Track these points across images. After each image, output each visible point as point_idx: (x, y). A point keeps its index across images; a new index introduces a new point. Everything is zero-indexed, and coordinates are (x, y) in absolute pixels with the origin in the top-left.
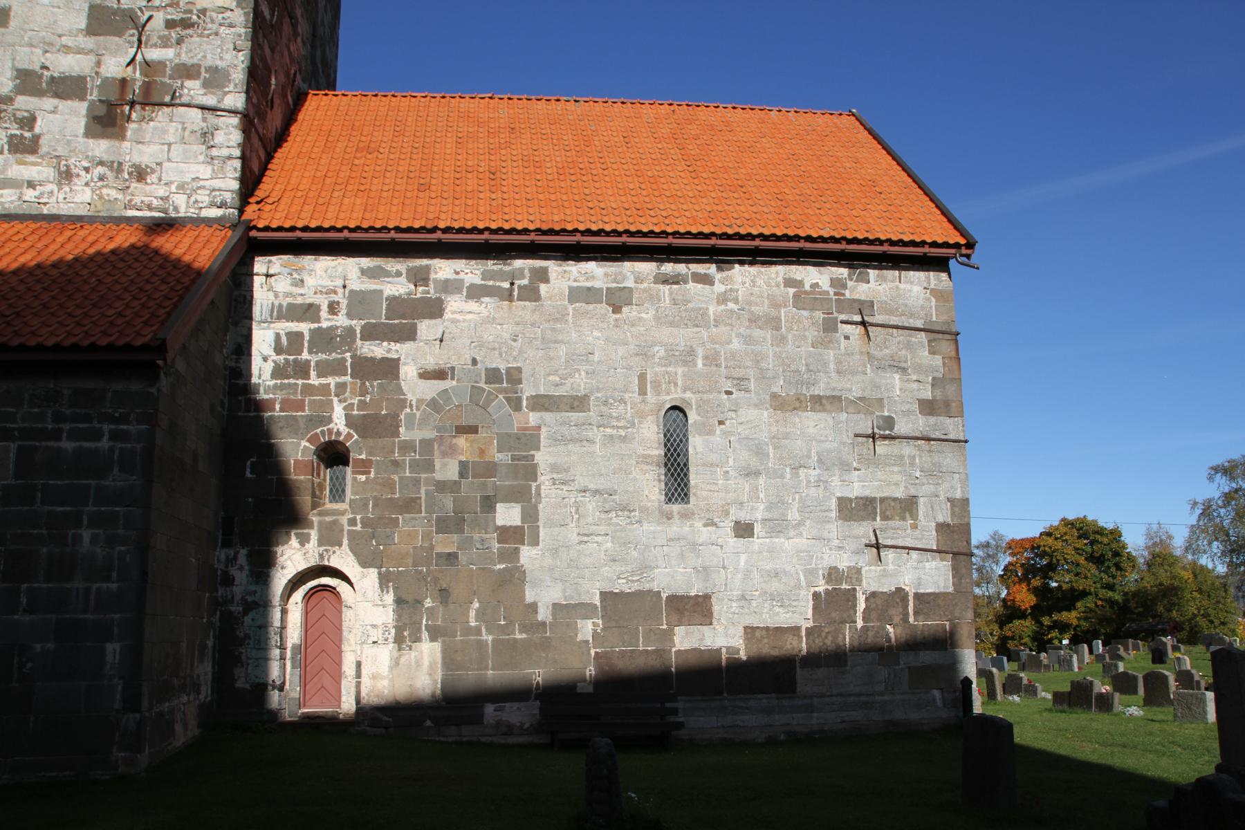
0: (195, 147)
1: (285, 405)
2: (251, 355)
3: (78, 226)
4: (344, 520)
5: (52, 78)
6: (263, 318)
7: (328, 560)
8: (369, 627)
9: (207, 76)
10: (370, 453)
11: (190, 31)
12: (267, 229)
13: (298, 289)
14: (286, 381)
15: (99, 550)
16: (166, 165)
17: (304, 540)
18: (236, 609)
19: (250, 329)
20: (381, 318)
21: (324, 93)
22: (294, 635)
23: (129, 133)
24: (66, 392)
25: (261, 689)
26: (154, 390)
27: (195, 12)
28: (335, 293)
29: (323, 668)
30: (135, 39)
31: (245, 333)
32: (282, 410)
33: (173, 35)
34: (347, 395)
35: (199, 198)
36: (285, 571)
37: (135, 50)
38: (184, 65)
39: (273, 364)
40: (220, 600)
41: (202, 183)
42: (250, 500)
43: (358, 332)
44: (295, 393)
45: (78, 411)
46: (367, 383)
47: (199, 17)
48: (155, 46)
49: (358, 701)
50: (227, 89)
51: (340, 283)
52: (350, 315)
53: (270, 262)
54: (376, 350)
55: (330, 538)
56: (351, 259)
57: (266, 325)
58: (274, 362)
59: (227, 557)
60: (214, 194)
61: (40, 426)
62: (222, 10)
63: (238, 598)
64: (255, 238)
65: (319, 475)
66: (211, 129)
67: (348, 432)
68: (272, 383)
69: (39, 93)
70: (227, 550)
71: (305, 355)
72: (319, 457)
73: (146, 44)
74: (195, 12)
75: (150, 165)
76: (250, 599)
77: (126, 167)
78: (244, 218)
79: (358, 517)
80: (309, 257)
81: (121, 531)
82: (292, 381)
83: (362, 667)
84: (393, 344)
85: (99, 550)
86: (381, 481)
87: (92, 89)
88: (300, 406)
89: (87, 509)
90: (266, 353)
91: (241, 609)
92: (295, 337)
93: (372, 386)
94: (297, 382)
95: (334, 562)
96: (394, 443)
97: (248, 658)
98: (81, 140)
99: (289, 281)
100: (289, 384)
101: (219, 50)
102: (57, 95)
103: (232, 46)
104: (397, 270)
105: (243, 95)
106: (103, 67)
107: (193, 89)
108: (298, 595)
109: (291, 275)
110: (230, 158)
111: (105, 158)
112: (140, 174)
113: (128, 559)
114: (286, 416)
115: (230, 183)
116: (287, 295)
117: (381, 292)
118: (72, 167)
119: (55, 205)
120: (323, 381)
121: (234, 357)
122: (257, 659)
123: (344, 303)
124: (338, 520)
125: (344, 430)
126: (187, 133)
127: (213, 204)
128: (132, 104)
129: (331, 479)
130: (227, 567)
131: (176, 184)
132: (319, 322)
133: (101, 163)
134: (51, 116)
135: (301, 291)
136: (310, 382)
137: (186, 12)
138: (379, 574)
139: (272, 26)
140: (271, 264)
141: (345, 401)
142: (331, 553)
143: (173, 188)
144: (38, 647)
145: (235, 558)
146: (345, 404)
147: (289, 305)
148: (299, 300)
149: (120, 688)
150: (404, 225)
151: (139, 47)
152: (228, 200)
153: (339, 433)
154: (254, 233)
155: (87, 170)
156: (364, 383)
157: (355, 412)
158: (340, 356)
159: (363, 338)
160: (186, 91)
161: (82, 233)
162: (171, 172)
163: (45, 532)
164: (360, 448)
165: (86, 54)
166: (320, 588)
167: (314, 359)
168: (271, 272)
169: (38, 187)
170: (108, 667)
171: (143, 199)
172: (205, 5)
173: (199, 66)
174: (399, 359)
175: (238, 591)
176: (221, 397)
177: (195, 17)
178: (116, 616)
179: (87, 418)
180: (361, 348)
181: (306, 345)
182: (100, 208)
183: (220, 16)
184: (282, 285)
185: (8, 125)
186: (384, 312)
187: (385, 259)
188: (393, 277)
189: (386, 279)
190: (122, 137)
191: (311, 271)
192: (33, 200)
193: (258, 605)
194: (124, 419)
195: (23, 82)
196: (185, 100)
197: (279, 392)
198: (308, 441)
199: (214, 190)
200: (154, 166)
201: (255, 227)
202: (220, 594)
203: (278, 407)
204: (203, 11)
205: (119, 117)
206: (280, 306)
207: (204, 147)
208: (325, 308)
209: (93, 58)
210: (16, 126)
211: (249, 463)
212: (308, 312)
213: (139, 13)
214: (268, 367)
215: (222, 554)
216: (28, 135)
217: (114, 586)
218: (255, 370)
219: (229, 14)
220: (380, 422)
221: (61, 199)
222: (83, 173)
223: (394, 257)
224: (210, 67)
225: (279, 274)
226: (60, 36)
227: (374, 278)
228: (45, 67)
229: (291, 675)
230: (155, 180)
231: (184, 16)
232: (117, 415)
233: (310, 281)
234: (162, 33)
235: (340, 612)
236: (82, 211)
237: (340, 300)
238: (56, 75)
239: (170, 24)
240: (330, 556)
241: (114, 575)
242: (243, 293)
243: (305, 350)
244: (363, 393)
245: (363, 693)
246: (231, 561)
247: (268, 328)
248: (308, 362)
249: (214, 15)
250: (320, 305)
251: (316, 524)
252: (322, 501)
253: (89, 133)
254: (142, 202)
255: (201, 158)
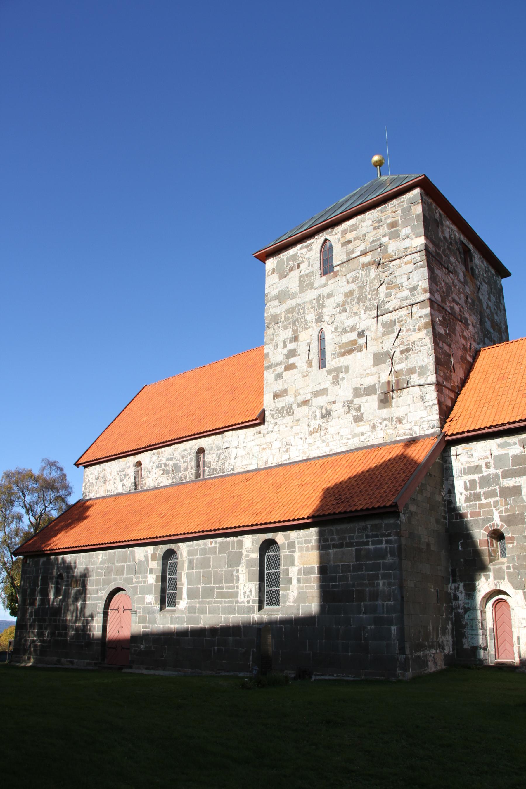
0: (419, 403)
1: (473, 514)
2: (455, 493)
3: (379, 449)
4: (504, 567)
5: (365, 388)
6: (458, 475)
7: (499, 587)
8: (521, 619)
9: (419, 371)
10: (513, 533)
11: (410, 353)
12: (452, 435)
13: (471, 459)
14: (471, 503)
15: (386, 588)
16: (409, 414)
17: (487, 577)
18: (461, 611)
19: (453, 481)
20: (510, 467)
21: (488, 348)
22: (489, 623)
23: (393, 404)
24: (369, 526)
25: (475, 649)
26: (398, 522)
27: (411, 344)
28: (487, 458)
29: (505, 640)
30: (390, 363)
31: (451, 483)
32: (471, 517)
33: (404, 356)
34: (499, 506)
35: (424, 426)
36: (480, 593)
37: (391, 367)
38: (410, 368)
39: (465, 496)
40: (454, 607)
41: (424, 419)
42: (462, 560)
43: (500, 475)
44: (476, 508)
45: (374, 533)
46: (508, 499)
47: (412, 346)
48: (398, 363)
49: (520, 657)
50: (427, 375)
51: (489, 453)
52: (495, 468)
53: (457, 448)
54: (509, 482)
55: (499, 576)
56: (492, 440)
57: (459, 478)
58: (465, 495)
59: (455, 587)
60: (429, 423)
61: (362, 540)
62: (421, 339)
63: (461, 606)
64: (449, 440)
65: (492, 546)
66: (424, 394)
67: (502, 524)
68: (465, 505)
69: (361, 396)
70: (455, 584)
71: (478, 490)
72: (491, 537)
73: (395, 363)
74: (411, 344)
75: (403, 416)
76: (466, 606)
77: (394, 419)
78: (443, 431)
79: (511, 565)
80: (474, 443)
81: (392, 581)
82: (474, 503)
83: (520, 639)
84: (517, 478)
85: (386, 588)
86: (519, 547)
87: (378, 389)
88: (479, 514)
89: (380, 572)
90: (461, 491)
91: (463, 611)
92: (472, 482)
93: (510, 500)
94: (476, 503)
95: (502, 588)
96: (523, 527)
97: (468, 634)
98: (377, 411)
99: (466, 456)
100: (473, 504)
101: (422, 358)
102: (367, 395)
103: (427, 355)
104: (514, 442)
105: (435, 375)
106: (381, 378)
107: (415, 379)
108: (490, 604)
109: (467, 453)
110: (433, 405)
111: (387, 417)
112: (400, 421)
113: (396, 592)
114: (474, 519)
115: (435, 416)
116: (467, 462)
117: (508, 454)
118: (375, 423)
119: (372, 441)
120: (488, 501)
121: (448, 495)
122: (472, 635)
123: (492, 462)
124: (502, 567)
125: (500, 523)
126: (415, 398)
127: (429, 427)
128: (393, 391)
129: (501, 547)
130: (455, 592)
131: (414, 422)
132: (482, 473)
133: (385, 419)
134: (366, 404)
135: (472, 460)
136: (482, 502)
137: (407, 345)
138: (524, 592)
139: (447, 335)
140: (458, 450)
141: (499, 509)
142: (500, 583)
143: (413, 425)
144: (369, 627)
145: (458, 588)
146: (498, 511)
147: (468, 467)
148: (472, 464)
149: (397, 644)
150: (511, 421)
151: (392, 366)
152: (435, 424)
153: (497, 525)
154: (447, 438)
155: (381, 423)
156: (506, 500)
157: (504, 514)
158: (493, 488)
159: (503, 478)
160: (412, 380)
161: (381, 451)
162: (412, 417)
163: (367, 582)
164: (508, 531)
165: (374, 375)
166: (500, 600)
167: (482, 491)
168: (458, 454)
169: (365, 435)
170: (393, 635)
171: (402, 431)
172: (414, 340)
173: (415, 367)
174: (521, 486)
175: (461, 603)
176: (443, 514)
177: (411, 346)
178: (394, 615)
179: (377, 536)
180: (503, 482)
181: (478, 485)
182: (387, 438)
183: (420, 342)
184: (464, 458)
185: (352, 412)
186: (511, 463)
187: (508, 437)
188: (513, 445)
189: (510, 447)
190: (391, 406)
191: (476, 449)
192: (364, 440)
193: (471, 609)
194: (389, 535)
195: (356, 393)
196: (412, 384)
197: (469, 509)
198: (484, 530)
199: (429, 421)
200: (404, 416)
201: (447, 435)
202: (453, 604)
203: (469, 516)
204: (414, 343)
205: (389, 398)
206: (464, 468)
207: (422, 403)
208: (484, 466)
209: (377, 375)
210: (355, 411)
211: (460, 543)
212: (477, 469)
213: (391, 351)
214: (463, 498)
215: (452, 586)
216: (359, 414)
217: (392, 603)
218: (457, 500)
219: (424, 340)
220: (516, 518)
221: (373, 438)
222: (379, 425)
223: (512, 436)
224: (420, 367)
225: (462, 453)
226: (365, 370)
227: (504, 447)
228: (362, 385)
229: (490, 643)
230: (406, 422)
231: (407, 347)
232: (387, 533)
233: (476, 455)
234: (400, 357)
235: (510, 611)
236: (381, 441)
237: (490, 461)
238: (365, 387)
239: (402, 352)
240: (500, 585)
241: (392, 598)
242: (448, 465)
243: (478, 487)
244: (506, 504)
245: (522, 653)
246: (457, 589)
247: (461, 479)
248: (480, 493)
249: (418, 343)
250: (481, 465)
251: (492, 570)
252: (497, 558)
253: (380, 408)
254: (402, 433)
255: (422, 408)
